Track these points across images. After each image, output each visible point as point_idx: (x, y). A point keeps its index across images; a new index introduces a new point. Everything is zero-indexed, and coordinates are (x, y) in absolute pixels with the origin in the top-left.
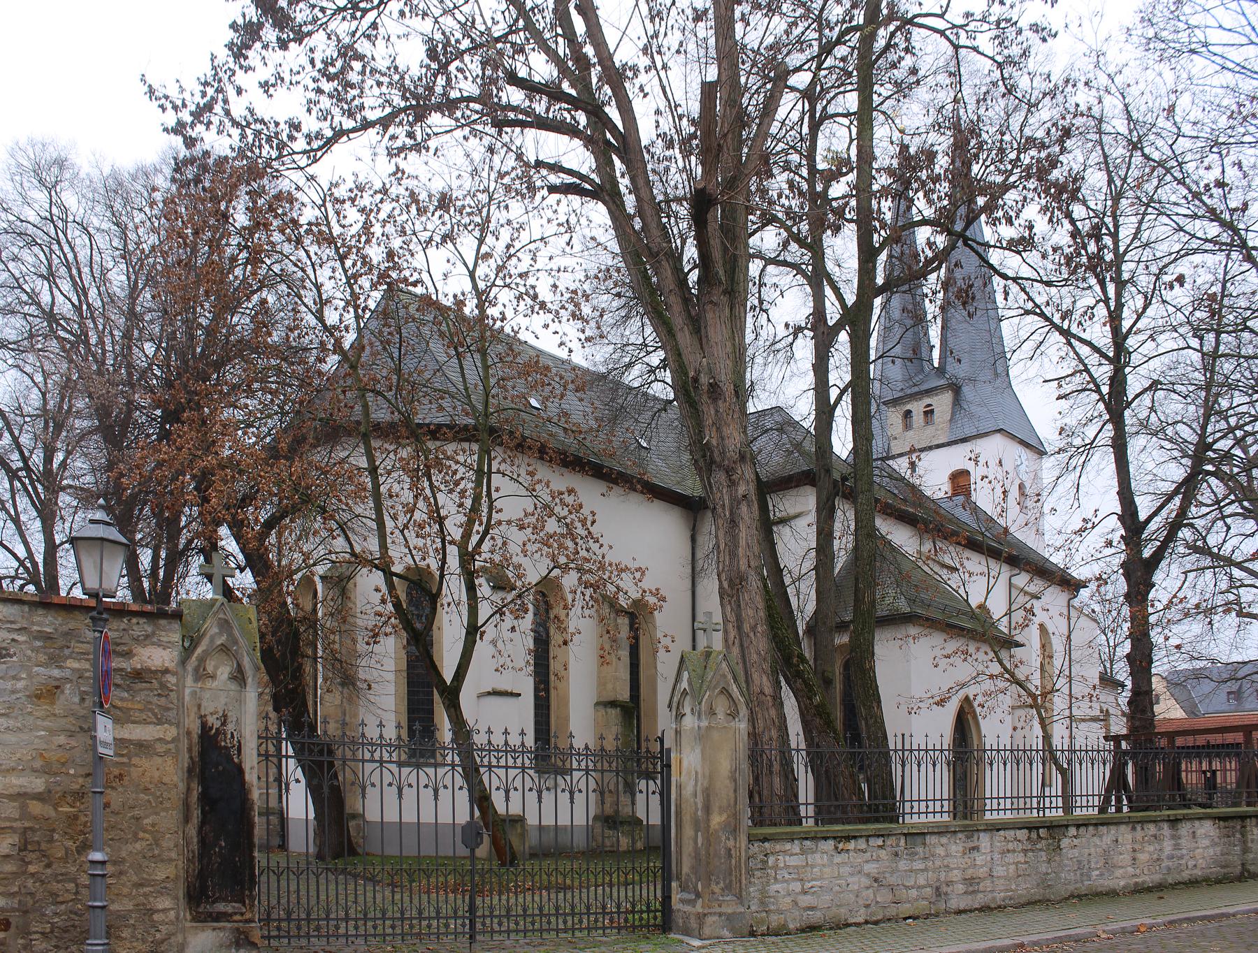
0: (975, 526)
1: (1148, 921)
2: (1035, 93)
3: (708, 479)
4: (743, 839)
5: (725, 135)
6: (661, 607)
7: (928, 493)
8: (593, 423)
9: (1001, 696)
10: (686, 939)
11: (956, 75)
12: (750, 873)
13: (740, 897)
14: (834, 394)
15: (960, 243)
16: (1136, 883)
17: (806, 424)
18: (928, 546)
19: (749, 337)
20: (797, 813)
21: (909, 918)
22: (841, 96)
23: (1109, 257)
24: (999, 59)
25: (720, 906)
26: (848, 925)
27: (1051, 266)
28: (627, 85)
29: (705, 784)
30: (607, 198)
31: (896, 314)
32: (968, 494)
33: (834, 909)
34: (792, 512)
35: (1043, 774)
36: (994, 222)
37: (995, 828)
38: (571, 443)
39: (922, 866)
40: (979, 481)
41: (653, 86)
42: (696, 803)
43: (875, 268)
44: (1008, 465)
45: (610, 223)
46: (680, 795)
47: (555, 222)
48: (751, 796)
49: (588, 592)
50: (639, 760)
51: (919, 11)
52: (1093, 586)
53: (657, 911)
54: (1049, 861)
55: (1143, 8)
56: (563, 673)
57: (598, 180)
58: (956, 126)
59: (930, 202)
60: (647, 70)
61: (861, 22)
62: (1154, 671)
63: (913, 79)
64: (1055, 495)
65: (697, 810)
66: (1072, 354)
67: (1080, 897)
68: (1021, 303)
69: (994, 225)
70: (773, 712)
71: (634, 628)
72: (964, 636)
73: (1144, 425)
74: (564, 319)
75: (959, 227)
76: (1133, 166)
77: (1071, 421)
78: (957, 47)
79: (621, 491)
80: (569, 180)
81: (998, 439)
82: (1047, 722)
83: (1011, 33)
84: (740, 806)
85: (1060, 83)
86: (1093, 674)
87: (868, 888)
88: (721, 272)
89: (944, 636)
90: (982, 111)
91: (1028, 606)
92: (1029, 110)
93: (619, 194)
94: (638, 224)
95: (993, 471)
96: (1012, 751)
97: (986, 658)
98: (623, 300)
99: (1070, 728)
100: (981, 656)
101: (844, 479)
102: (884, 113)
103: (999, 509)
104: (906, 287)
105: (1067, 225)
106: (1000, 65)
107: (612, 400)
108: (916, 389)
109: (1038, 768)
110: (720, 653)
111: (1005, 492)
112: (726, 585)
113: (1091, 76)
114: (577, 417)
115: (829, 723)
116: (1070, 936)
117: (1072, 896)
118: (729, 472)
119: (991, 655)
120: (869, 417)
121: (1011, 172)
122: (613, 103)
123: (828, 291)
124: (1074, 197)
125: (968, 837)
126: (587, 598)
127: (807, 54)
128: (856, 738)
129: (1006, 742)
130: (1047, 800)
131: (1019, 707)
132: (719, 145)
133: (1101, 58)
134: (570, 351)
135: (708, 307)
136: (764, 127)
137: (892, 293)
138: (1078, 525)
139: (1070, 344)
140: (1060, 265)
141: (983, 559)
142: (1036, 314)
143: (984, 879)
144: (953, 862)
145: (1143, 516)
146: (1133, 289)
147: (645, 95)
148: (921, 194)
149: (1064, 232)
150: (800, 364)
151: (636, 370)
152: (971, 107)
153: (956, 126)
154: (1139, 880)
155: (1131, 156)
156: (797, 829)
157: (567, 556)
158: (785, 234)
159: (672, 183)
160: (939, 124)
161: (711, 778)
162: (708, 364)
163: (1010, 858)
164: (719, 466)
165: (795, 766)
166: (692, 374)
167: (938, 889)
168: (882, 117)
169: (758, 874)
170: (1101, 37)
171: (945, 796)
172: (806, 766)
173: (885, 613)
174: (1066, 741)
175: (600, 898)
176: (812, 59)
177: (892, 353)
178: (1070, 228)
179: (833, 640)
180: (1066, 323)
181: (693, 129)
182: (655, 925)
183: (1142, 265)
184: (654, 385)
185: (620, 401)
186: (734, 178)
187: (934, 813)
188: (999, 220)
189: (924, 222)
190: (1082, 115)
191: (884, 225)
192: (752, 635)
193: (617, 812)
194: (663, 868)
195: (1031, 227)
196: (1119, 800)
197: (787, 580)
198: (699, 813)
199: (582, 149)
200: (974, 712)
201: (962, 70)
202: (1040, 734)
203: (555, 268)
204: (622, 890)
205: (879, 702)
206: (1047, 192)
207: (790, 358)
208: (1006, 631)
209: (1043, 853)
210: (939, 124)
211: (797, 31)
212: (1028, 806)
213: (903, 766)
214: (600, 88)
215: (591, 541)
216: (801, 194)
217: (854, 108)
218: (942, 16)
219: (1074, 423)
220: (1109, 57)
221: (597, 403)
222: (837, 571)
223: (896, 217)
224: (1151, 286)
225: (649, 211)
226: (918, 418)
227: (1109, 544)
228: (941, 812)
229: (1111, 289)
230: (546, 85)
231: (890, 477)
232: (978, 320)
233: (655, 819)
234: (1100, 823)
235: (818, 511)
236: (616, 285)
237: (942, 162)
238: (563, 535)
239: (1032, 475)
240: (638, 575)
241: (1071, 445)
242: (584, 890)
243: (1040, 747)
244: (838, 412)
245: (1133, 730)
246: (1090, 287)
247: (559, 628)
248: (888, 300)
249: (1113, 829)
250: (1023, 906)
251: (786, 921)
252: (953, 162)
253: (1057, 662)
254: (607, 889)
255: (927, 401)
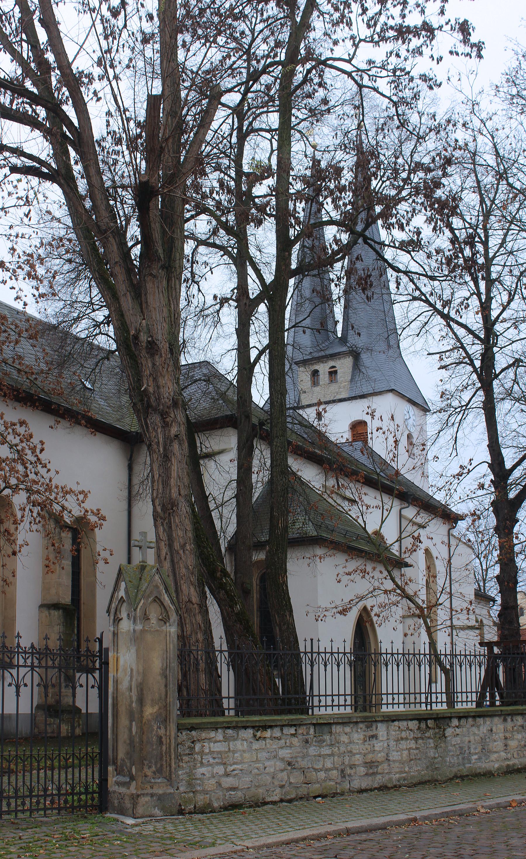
0: (371, 467)
1: (518, 798)
2: (423, 128)
3: (145, 420)
4: (173, 727)
5: (167, 140)
6: (101, 525)
7: (333, 439)
8: (43, 366)
9: (394, 608)
10: (121, 818)
11: (360, 107)
12: (179, 757)
13: (169, 779)
14: (253, 354)
15: (360, 240)
16: (508, 766)
17: (230, 377)
18: (332, 482)
19: (183, 303)
20: (220, 705)
21: (319, 796)
22: (264, 115)
23: (481, 260)
24: (395, 99)
25: (152, 787)
26: (265, 803)
27: (434, 265)
28: (83, 89)
29: (140, 679)
30: (62, 181)
31: (307, 293)
32: (365, 441)
33: (253, 789)
34: (216, 448)
35: (430, 674)
36: (388, 227)
37: (391, 719)
38: (24, 382)
39: (329, 752)
40: (374, 431)
41: (106, 93)
42: (131, 697)
43: (290, 255)
44: (399, 420)
45: (63, 201)
46: (116, 689)
47: (15, 196)
48: (180, 690)
49: (36, 510)
50: (79, 658)
51: (330, 56)
52: (469, 520)
53: (94, 792)
54: (436, 747)
55: (508, 71)
56: (10, 579)
57: (54, 165)
58: (359, 148)
59: (337, 207)
60: (101, 78)
61: (283, 57)
62: (518, 589)
63: (324, 108)
64: (437, 445)
65: (132, 702)
66: (451, 334)
67: (462, 777)
68: (410, 291)
69: (389, 229)
70: (199, 618)
71: (75, 541)
72: (362, 557)
73: (509, 393)
74: (21, 277)
75: (359, 228)
76: (500, 191)
77: (451, 387)
78: (361, 87)
79: (68, 424)
80: (29, 163)
81: (390, 397)
82: (432, 630)
83: (404, 81)
84: (170, 699)
85: (443, 122)
86: (470, 592)
87: (282, 771)
88: (160, 251)
89: (347, 557)
90: (380, 138)
91: (416, 535)
92: (418, 141)
93: (73, 179)
94: (88, 204)
95: (386, 424)
96: (403, 654)
97: (381, 576)
98: (74, 265)
99: (451, 635)
100: (377, 574)
101: (262, 424)
102: (300, 132)
103: (391, 455)
104: (315, 272)
105: (448, 233)
106: (395, 104)
107: (62, 347)
108: (323, 353)
109: (425, 669)
110: (153, 567)
111: (396, 442)
112: (159, 509)
113: (468, 119)
114: (29, 361)
115: (248, 628)
116: (455, 811)
117: (456, 777)
118: (164, 415)
119: (385, 573)
120: (283, 374)
121: (403, 188)
122: (70, 102)
123: (250, 271)
124: (454, 211)
125: (367, 727)
126: (35, 515)
127: (238, 79)
128: (271, 641)
129: (398, 647)
130: (434, 696)
131: (409, 616)
132: (161, 147)
133: (476, 107)
134: (25, 304)
135: (148, 279)
136: (200, 136)
137: (304, 276)
138: (458, 470)
139: (449, 326)
140: (442, 263)
141: (377, 494)
142: (421, 300)
143: (382, 762)
144: (355, 748)
145: (508, 465)
146: (500, 287)
147: (99, 99)
148: (329, 200)
149: (445, 238)
150: (225, 328)
151: (84, 323)
152: (371, 134)
153: (359, 148)
154: (510, 763)
155: (498, 184)
156: (220, 719)
157: (18, 479)
158: (214, 223)
159: (120, 173)
160: (345, 145)
161: (145, 673)
162: (147, 325)
163: (404, 745)
164: (155, 410)
165: (219, 665)
166: (133, 332)
167: (342, 771)
168: (298, 136)
169: (186, 758)
170: (476, 90)
171: (348, 692)
172: (228, 665)
173: (296, 536)
174: (449, 646)
175: (42, 781)
176: (241, 84)
177: (303, 324)
178: (450, 236)
179: (251, 557)
180: (446, 309)
181: (139, 130)
182: (92, 806)
183: (507, 269)
184: (99, 337)
185: (68, 348)
186: (173, 175)
187: (339, 706)
188: (393, 225)
189: (331, 222)
190: (460, 149)
191: (298, 222)
192: (181, 552)
193: (58, 702)
194: (100, 754)
195: (419, 233)
196: (492, 696)
197: (212, 506)
198: (134, 705)
199: (42, 138)
200: (372, 620)
201: (364, 103)
202: (427, 641)
203: (14, 234)
204: (63, 773)
205: (291, 611)
206: (431, 206)
207: (217, 322)
208: (397, 554)
209: (431, 741)
210: (345, 145)
211: (229, 62)
212: (418, 700)
213: (312, 666)
214: (59, 90)
215: (40, 466)
216: (229, 191)
217: (276, 125)
218: (349, 61)
219: (453, 389)
220: (482, 106)
221: (48, 350)
222: (254, 499)
223: (309, 215)
224: (514, 286)
225: (99, 196)
226: (324, 377)
227: (482, 486)
228: (345, 705)
229: (482, 285)
230: (11, 82)
231: (300, 424)
232: (375, 303)
233: (94, 708)
234: (475, 716)
235: (239, 449)
236: (67, 252)
237: (347, 177)
238: (14, 460)
239: (418, 428)
240: (81, 497)
241: (450, 406)
242: (27, 774)
243: (427, 652)
244: (257, 369)
245: (502, 636)
246: (466, 282)
247: (8, 540)
248: (301, 281)
249: (488, 721)
250: (415, 785)
251: (210, 800)
252: (356, 177)
253: (441, 580)
254: (49, 773)
255: (331, 363)
